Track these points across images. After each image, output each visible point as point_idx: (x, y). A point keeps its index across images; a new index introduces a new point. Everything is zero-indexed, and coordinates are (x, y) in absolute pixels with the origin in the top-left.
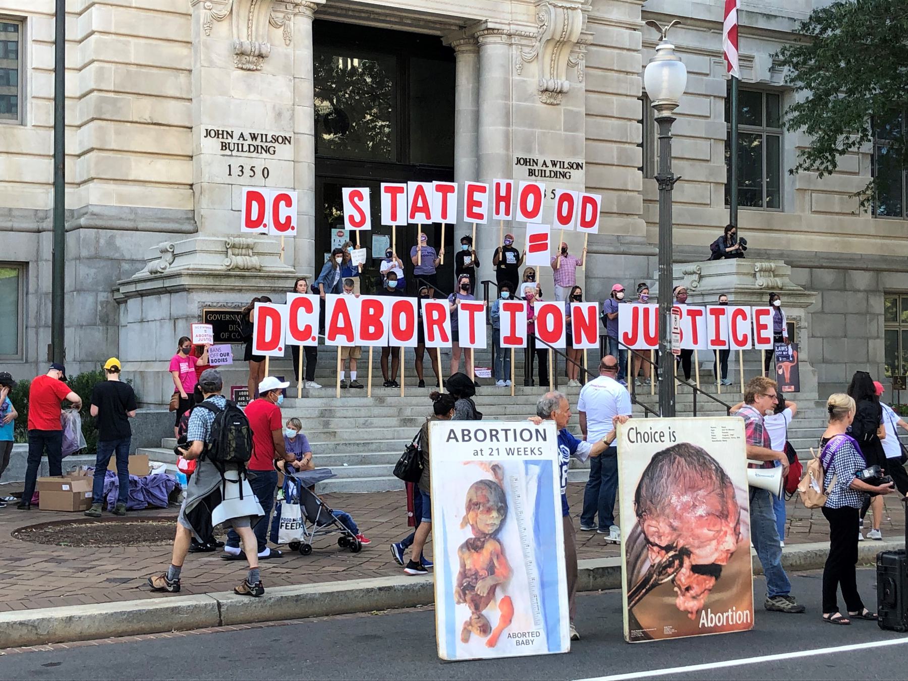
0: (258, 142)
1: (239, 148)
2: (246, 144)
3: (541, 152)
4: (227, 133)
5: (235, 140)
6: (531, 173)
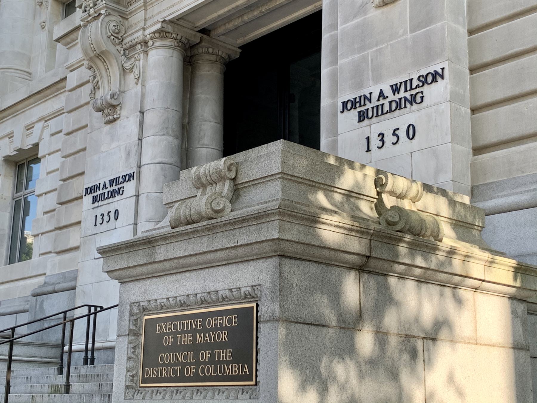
0: (402, 94)
1: (379, 111)
2: (386, 102)
3: (377, 79)
4: (365, 97)
5: (375, 103)
6: (362, 116)
